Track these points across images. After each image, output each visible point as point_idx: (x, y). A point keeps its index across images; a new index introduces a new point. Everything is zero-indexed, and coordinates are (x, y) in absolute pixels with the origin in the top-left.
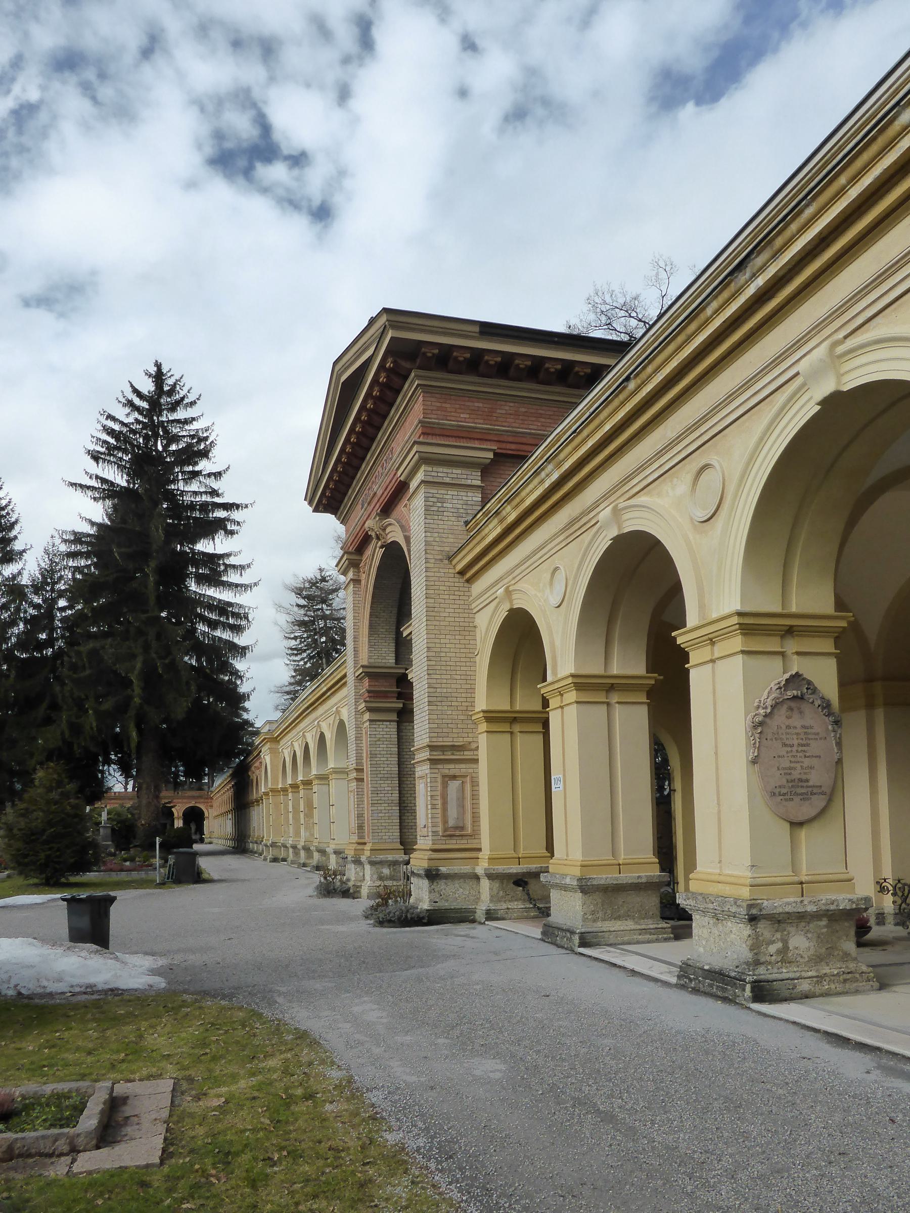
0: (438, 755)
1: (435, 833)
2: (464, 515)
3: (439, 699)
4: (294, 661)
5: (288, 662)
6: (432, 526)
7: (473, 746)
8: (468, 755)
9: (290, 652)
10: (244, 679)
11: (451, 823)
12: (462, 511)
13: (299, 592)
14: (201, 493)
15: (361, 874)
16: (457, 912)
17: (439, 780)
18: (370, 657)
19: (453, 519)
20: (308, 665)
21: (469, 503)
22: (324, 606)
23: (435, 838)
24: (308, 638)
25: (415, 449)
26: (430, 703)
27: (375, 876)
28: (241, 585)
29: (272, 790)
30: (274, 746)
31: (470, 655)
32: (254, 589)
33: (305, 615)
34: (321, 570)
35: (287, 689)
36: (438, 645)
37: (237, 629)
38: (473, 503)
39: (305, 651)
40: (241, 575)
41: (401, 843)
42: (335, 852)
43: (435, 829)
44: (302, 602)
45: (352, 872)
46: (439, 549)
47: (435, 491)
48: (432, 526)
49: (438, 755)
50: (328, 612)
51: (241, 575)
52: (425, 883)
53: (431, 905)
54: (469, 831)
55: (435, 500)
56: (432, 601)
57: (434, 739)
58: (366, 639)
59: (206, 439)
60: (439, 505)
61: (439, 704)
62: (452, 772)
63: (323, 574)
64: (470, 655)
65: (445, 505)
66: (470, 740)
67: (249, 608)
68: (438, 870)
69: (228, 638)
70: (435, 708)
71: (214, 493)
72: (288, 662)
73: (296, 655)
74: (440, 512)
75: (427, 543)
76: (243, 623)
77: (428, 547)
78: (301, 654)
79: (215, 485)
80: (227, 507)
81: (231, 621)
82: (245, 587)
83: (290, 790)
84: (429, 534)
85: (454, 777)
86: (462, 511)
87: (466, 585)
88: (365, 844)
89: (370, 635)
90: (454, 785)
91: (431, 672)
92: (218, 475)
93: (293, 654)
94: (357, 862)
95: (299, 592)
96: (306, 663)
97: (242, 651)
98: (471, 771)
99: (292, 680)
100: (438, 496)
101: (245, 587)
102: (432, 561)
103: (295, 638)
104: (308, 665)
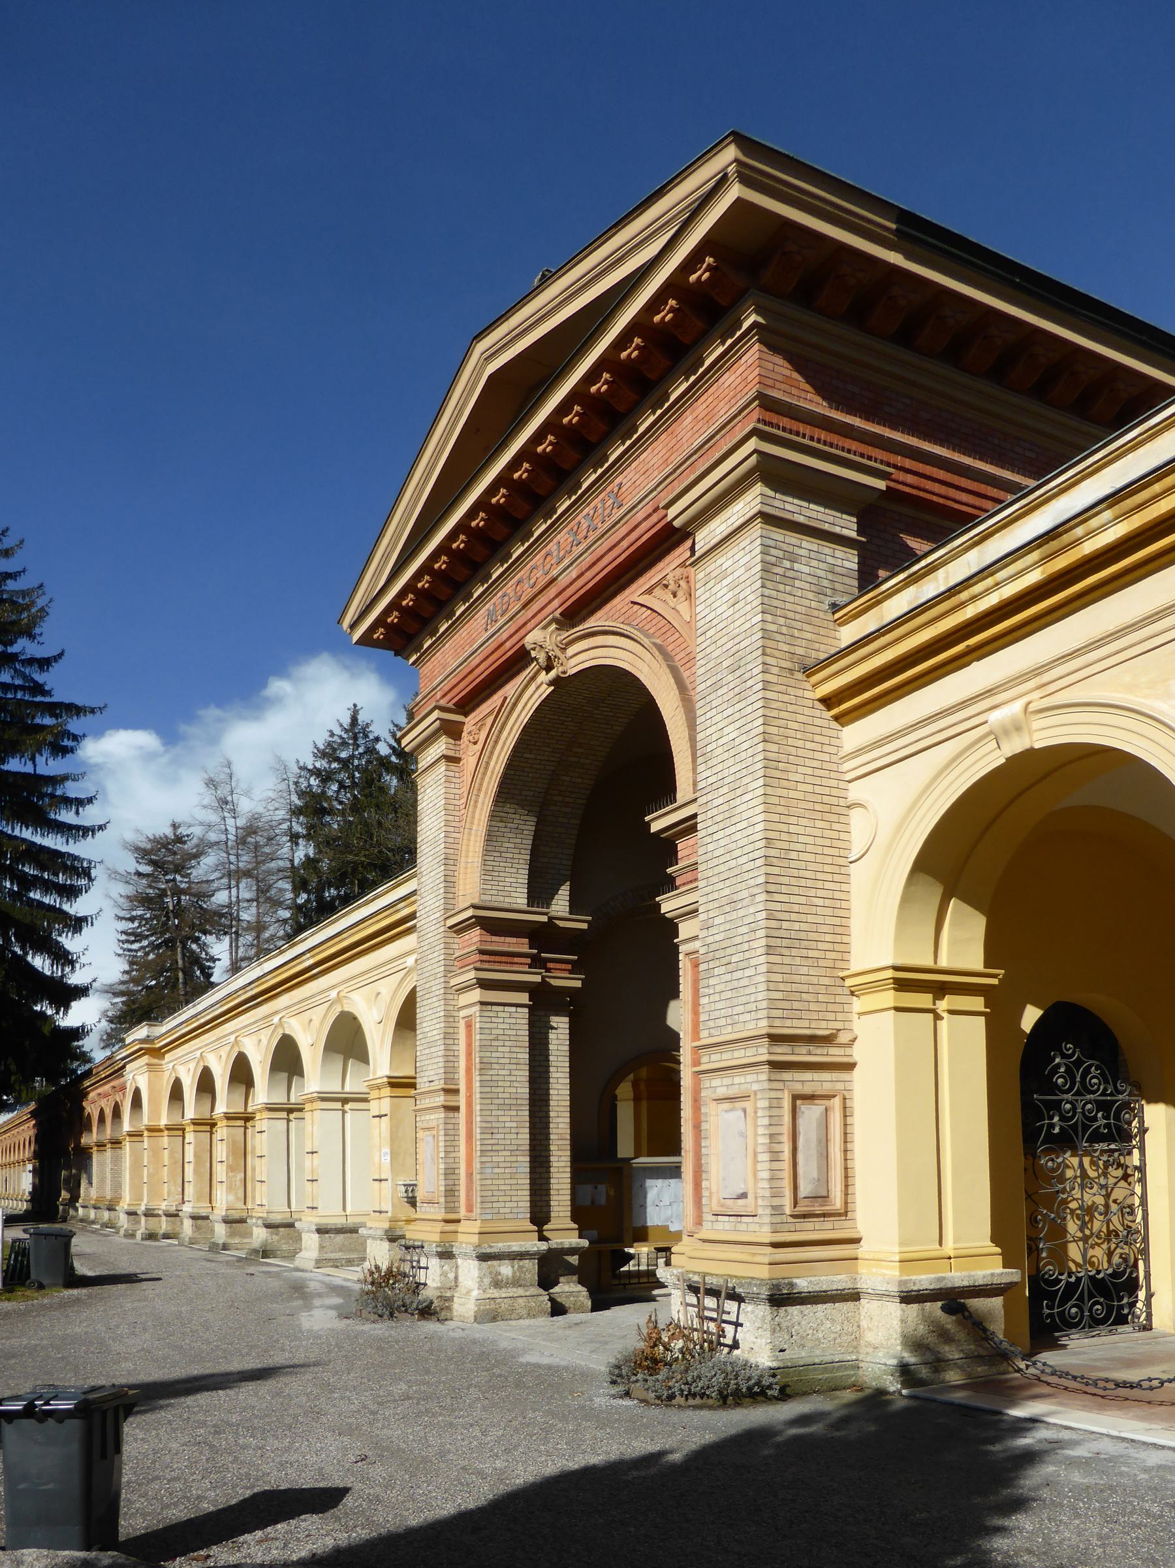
0: (784, 1053)
1: (777, 1210)
2: (829, 592)
3: (785, 943)
4: (130, 950)
5: (121, 952)
6: (776, 603)
7: (843, 1038)
8: (833, 1054)
9: (124, 937)
10: (77, 966)
11: (804, 1190)
12: (826, 583)
13: (143, 854)
14: (16, 688)
15: (451, 1276)
16: (825, 1370)
17: (786, 1103)
18: (484, 892)
19: (811, 595)
20: (151, 956)
21: (838, 570)
22: (178, 878)
23: (778, 1219)
24: (151, 919)
25: (752, 444)
26: (770, 950)
27: (487, 1281)
28: (78, 828)
29: (151, 1130)
30: (156, 1061)
31: (842, 861)
32: (99, 834)
33: (150, 887)
34: (175, 826)
35: (123, 987)
36: (784, 836)
37: (72, 893)
38: (844, 571)
39: (147, 937)
40: (77, 813)
41: (533, 1221)
42: (194, 1218)
43: (776, 1202)
44: (147, 869)
45: (432, 1275)
46: (786, 648)
47: (781, 538)
48: (776, 603)
49: (784, 1053)
50: (183, 886)
51: (77, 813)
52: (764, 1310)
53: (777, 1359)
54: (837, 1203)
55: (781, 554)
56: (774, 748)
57: (777, 1023)
58: (478, 860)
59: (27, 607)
60: (787, 564)
61: (785, 952)
62: (808, 1089)
63: (179, 831)
64: (842, 861)
65: (796, 566)
66: (839, 1025)
67: (90, 862)
68: (792, 1285)
69: (52, 903)
70: (777, 959)
71: (38, 689)
72: (121, 952)
73: (132, 942)
74: (789, 579)
75: (766, 635)
76: (83, 882)
77: (770, 643)
78: (139, 941)
79: (39, 677)
80: (55, 709)
81: (61, 879)
82: (86, 831)
83: (146, 1133)
84: (769, 618)
85: (811, 1098)
86: (826, 583)
87: (834, 725)
88: (458, 1221)
89: (487, 852)
90: (810, 1114)
91: (772, 888)
92: (44, 663)
93: (127, 941)
94: (446, 1255)
95: (143, 854)
96: (147, 954)
97: (77, 924)
98: (840, 1086)
99: (126, 977)
100: (785, 547)
101: (86, 831)
102: (775, 670)
103: (132, 919)
104: (151, 956)
